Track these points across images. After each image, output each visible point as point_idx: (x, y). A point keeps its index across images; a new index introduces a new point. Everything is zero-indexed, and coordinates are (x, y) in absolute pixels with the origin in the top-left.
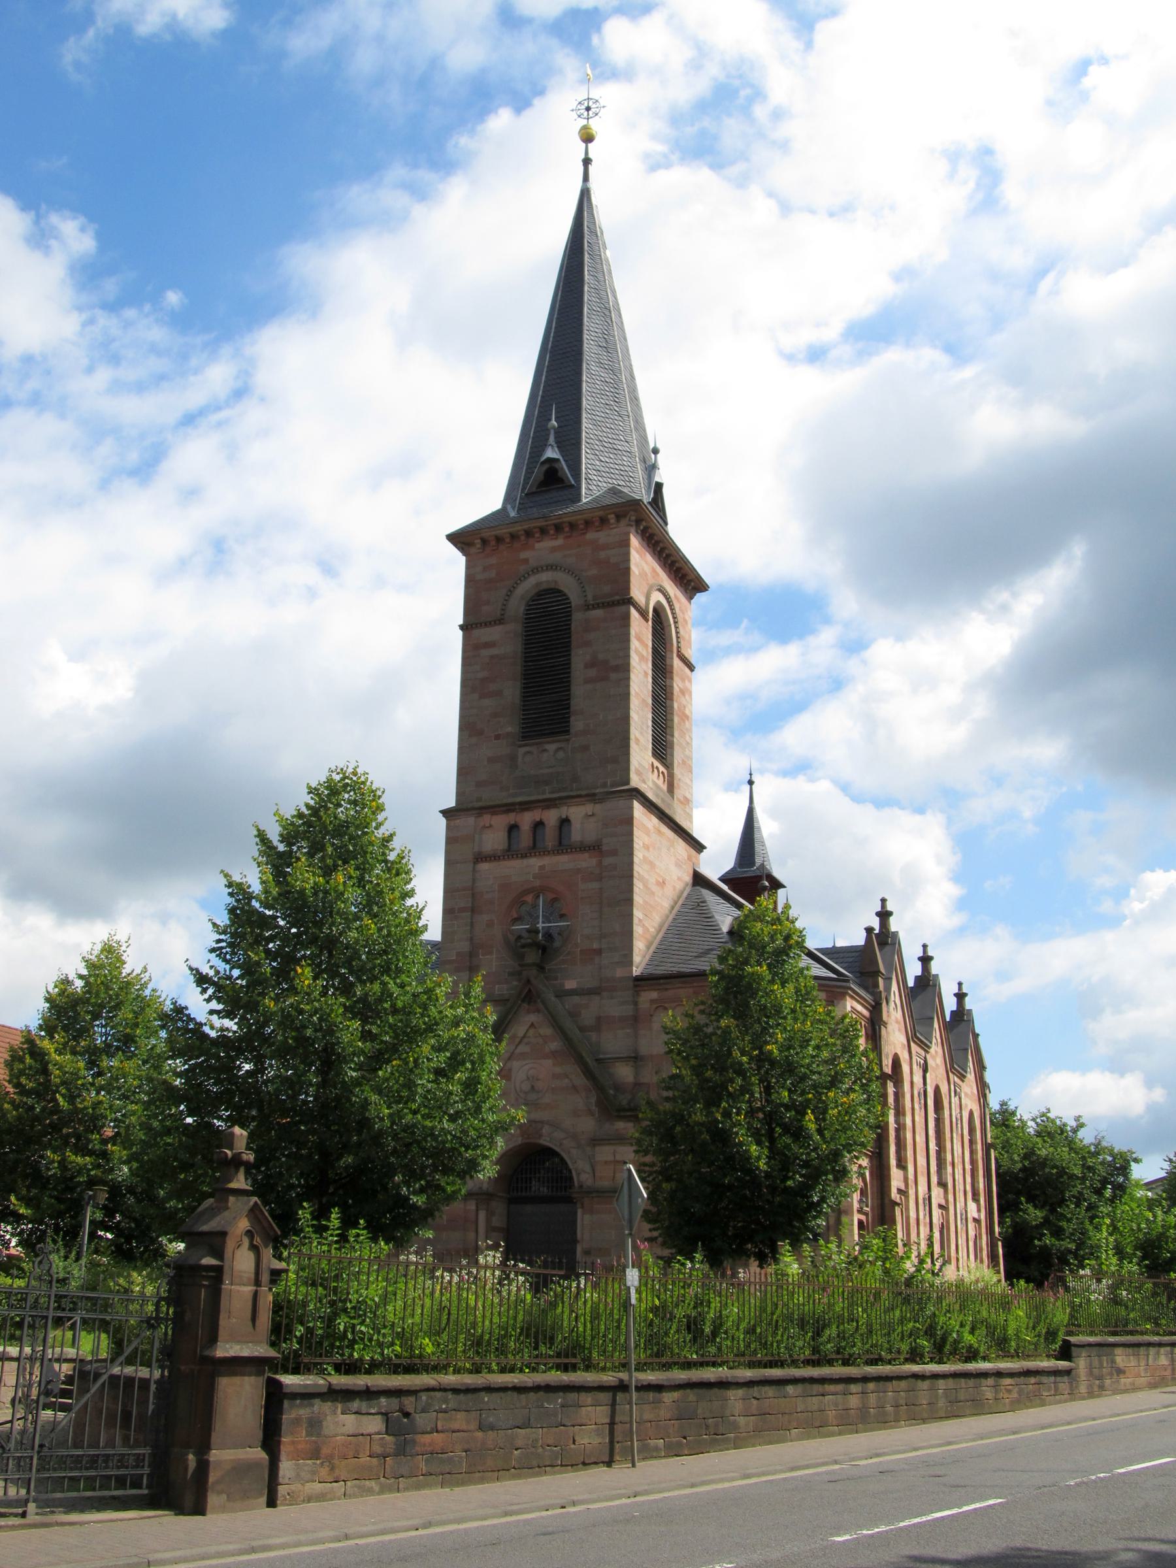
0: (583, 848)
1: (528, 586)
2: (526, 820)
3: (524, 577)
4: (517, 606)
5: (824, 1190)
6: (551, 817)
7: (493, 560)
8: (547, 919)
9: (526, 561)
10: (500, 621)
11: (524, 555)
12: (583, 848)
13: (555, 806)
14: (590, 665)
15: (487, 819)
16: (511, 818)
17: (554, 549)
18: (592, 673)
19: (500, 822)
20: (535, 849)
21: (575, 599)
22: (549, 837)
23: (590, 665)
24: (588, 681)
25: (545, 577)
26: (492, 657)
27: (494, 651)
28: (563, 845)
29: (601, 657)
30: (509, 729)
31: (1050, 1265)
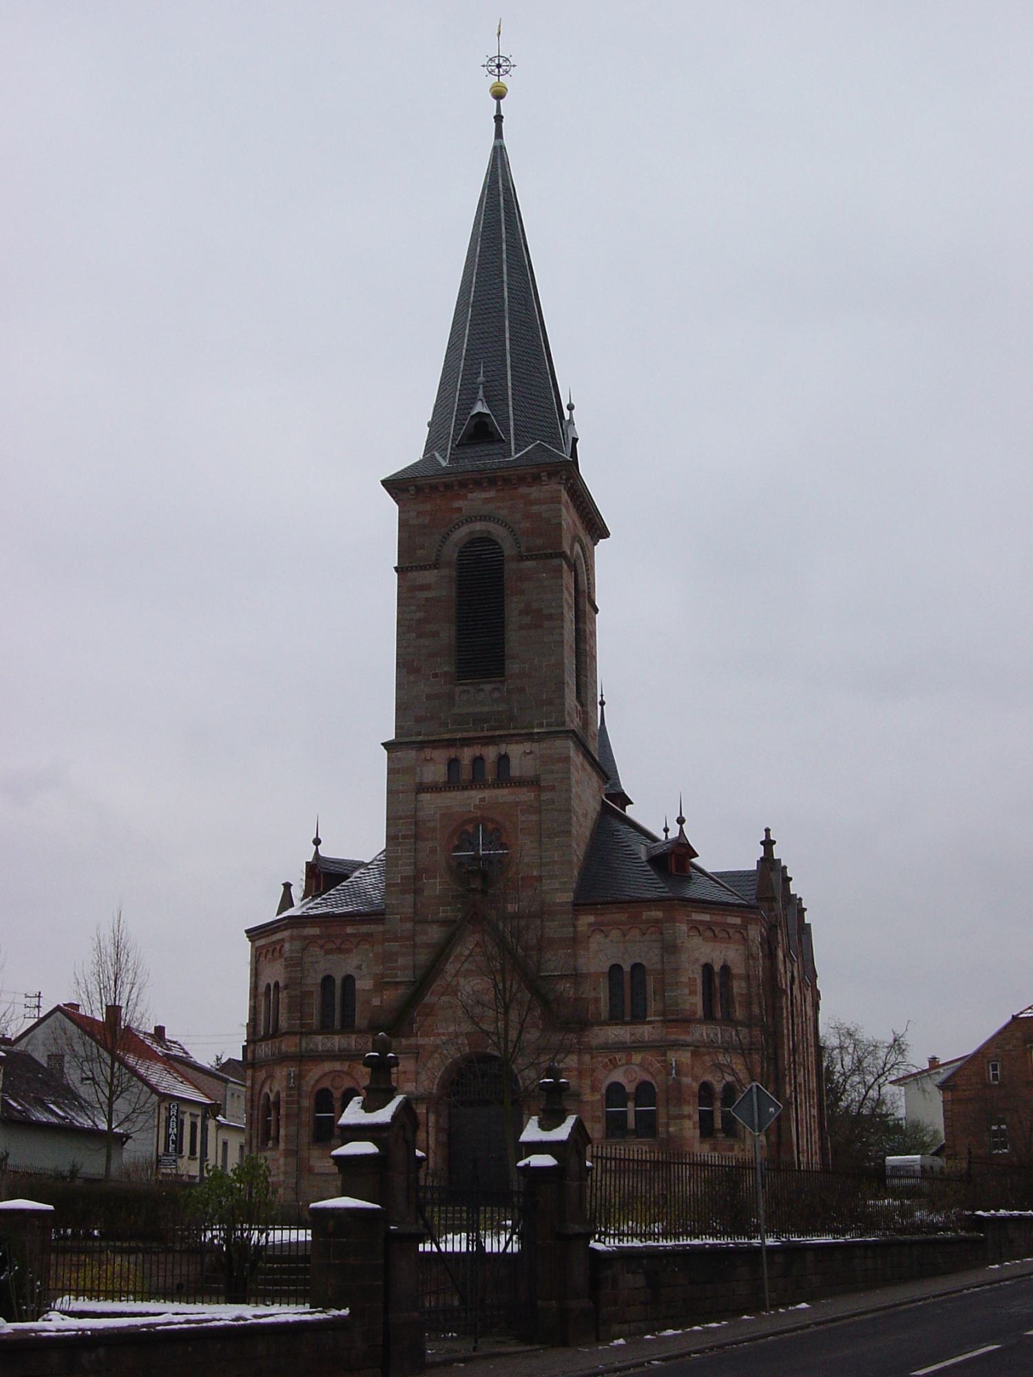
0: (521, 782)
1: (462, 533)
2: (467, 754)
3: (459, 525)
6: (491, 753)
12: (521, 782)
15: (428, 753)
16: (452, 753)
18: (527, 620)
19: (441, 755)
20: (477, 781)
21: (508, 549)
25: (478, 526)
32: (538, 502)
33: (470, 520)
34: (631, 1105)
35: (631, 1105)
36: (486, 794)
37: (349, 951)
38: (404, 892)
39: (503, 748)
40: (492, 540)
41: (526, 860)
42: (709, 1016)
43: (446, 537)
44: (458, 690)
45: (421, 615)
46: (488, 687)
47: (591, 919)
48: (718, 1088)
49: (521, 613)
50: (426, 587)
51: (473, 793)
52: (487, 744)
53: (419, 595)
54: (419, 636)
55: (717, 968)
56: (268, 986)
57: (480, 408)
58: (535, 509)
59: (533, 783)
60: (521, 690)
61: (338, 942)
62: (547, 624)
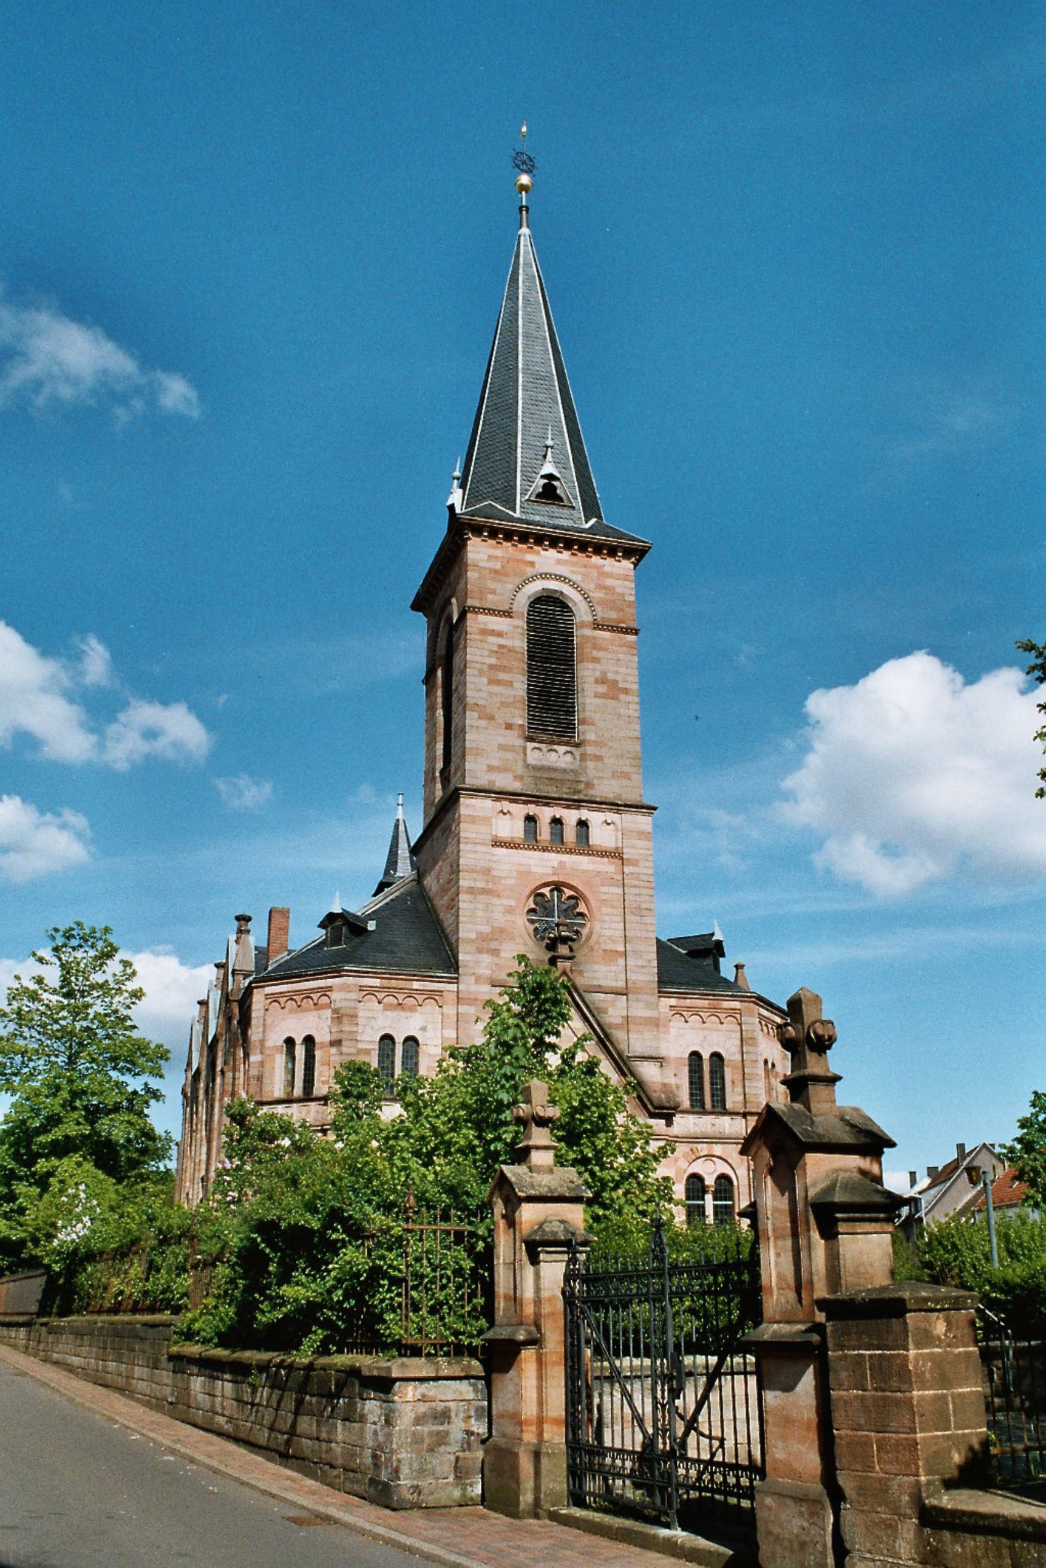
0: (604, 854)
1: (536, 587)
2: (545, 814)
3: (533, 578)
4: (522, 604)
5: (323, 1149)
6: (571, 817)
7: (498, 552)
8: (553, 917)
9: (532, 564)
10: (508, 614)
11: (529, 557)
12: (604, 854)
13: (578, 808)
14: (602, 681)
15: (506, 805)
16: (532, 809)
17: (559, 562)
18: (602, 689)
19: (520, 810)
20: (557, 842)
21: (582, 612)
22: (545, 832)
23: (602, 681)
24: (597, 695)
25: (553, 585)
26: (501, 646)
27: (502, 641)
28: (583, 843)
29: (610, 676)
30: (520, 722)
31: (41, 1177)
32: (611, 575)
33: (545, 576)
34: (709, 1198)
35: (709, 1198)
36: (566, 858)
37: (412, 1009)
38: (480, 951)
39: (584, 814)
40: (562, 602)
41: (608, 933)
42: (698, 1106)
43: (518, 589)
44: (530, 745)
45: (493, 661)
46: (562, 749)
47: (673, 1002)
48: (710, 1181)
49: (597, 681)
50: (500, 634)
51: (553, 855)
52: (568, 807)
53: (492, 639)
54: (490, 682)
55: (706, 1056)
56: (290, 1042)
57: (548, 468)
58: (609, 582)
59: (616, 855)
60: (598, 758)
61: (401, 997)
62: (622, 696)
